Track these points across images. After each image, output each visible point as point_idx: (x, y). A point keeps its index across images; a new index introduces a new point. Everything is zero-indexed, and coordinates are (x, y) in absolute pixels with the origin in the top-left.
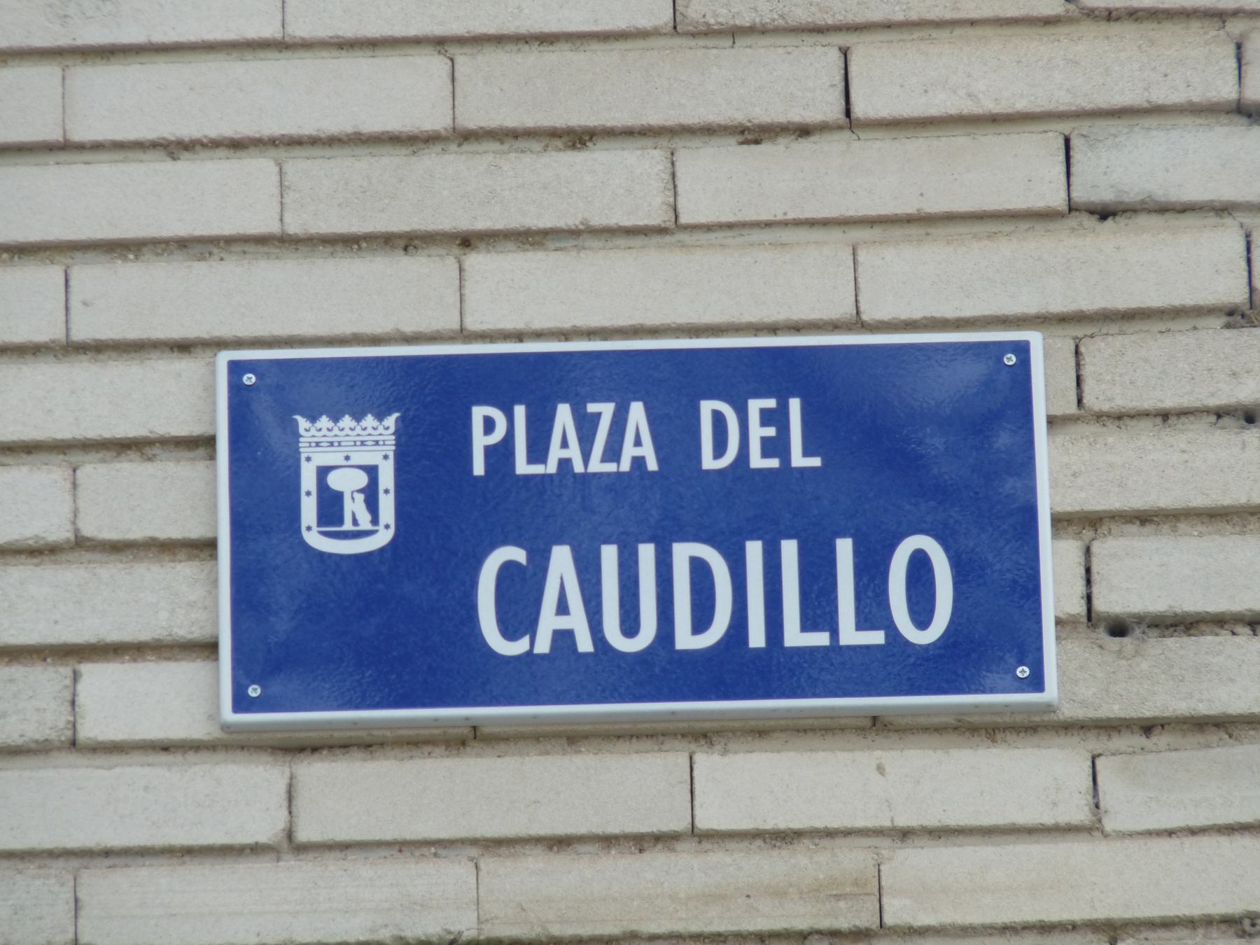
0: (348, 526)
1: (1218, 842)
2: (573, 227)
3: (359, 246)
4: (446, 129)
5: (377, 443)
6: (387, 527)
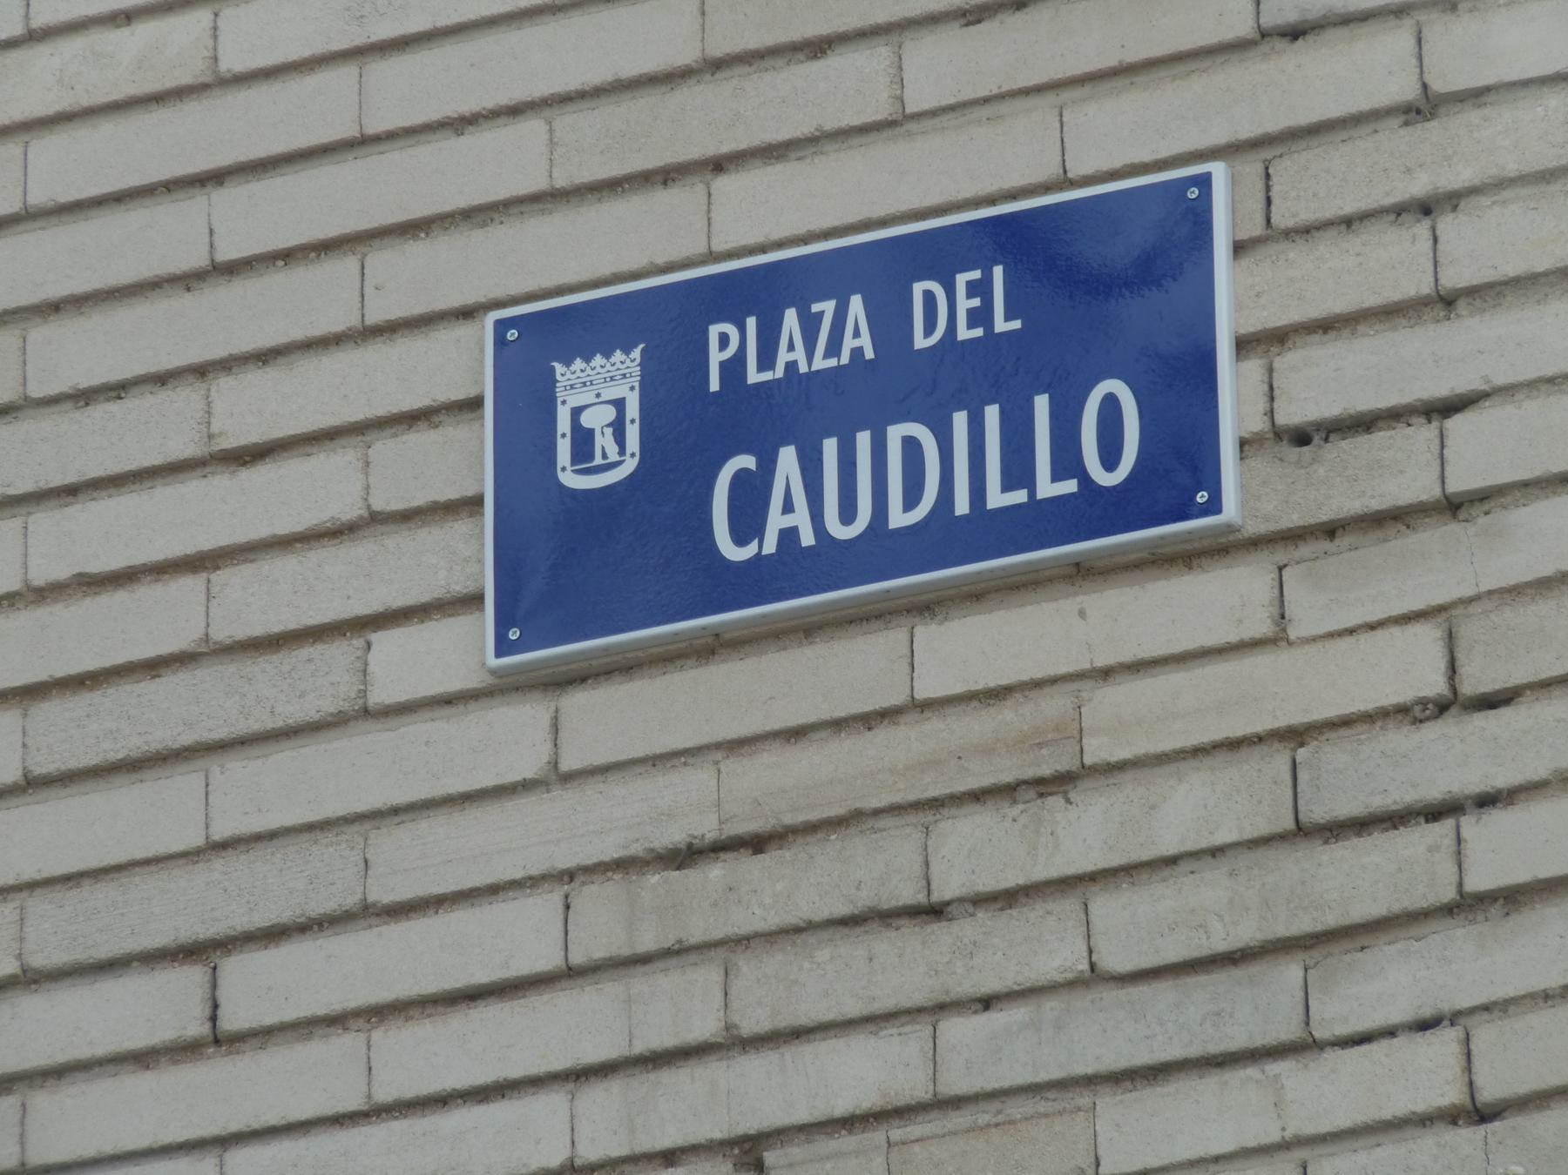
0: (598, 460)
1: (1390, 633)
2: (809, 135)
3: (623, 188)
4: (697, 62)
5: (624, 376)
6: (633, 455)
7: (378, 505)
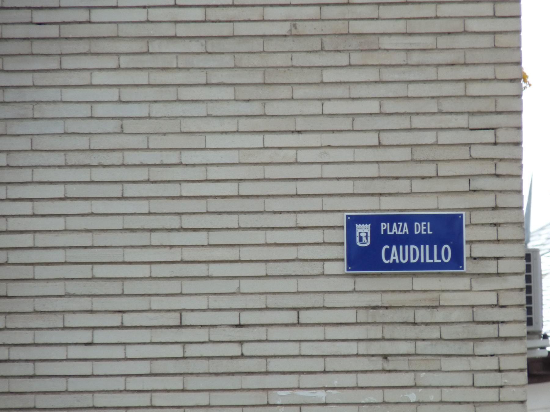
7: (326, 241)
